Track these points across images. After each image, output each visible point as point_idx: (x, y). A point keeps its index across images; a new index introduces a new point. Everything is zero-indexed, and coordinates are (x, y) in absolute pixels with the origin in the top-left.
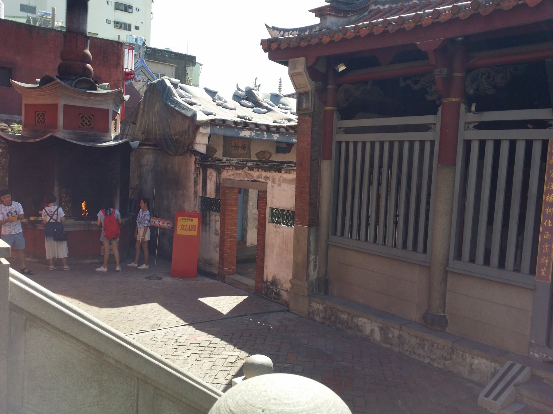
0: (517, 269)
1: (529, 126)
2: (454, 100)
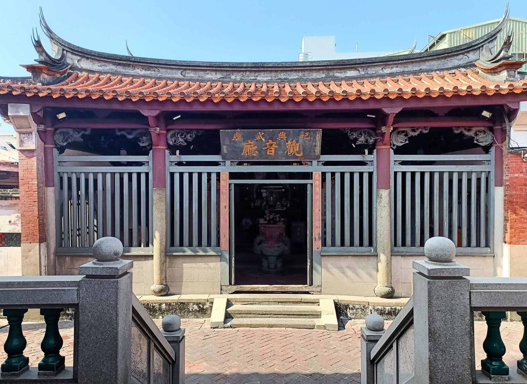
0: (478, 245)
1: (185, 163)
2: (162, 147)
